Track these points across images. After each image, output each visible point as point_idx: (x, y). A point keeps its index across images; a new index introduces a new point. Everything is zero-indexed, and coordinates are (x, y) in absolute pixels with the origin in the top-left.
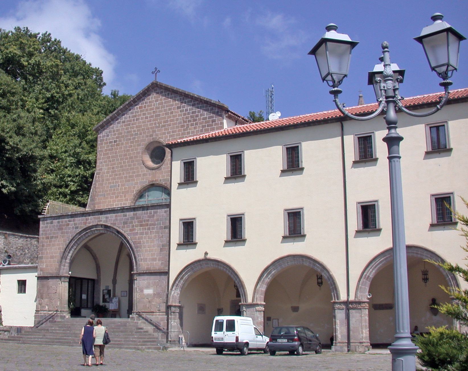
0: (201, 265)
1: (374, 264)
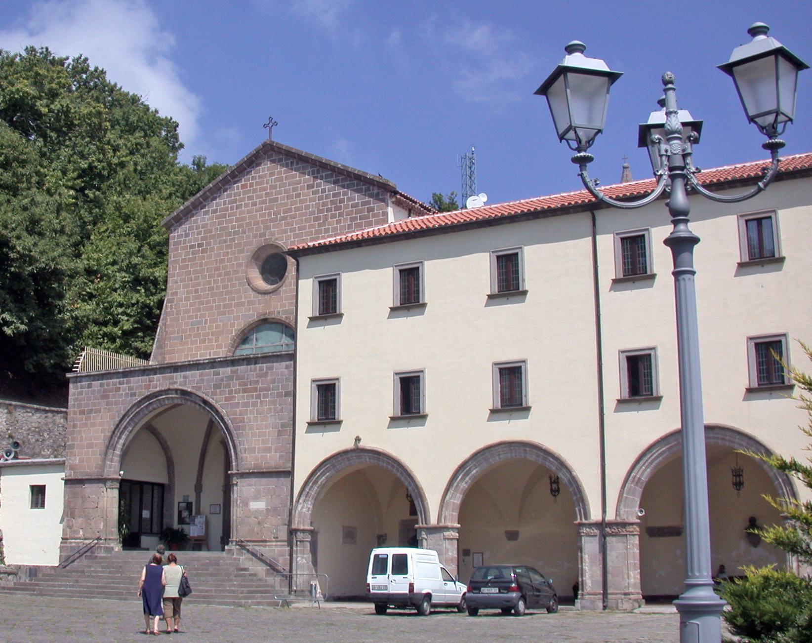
0: (348, 459)
1: (649, 458)
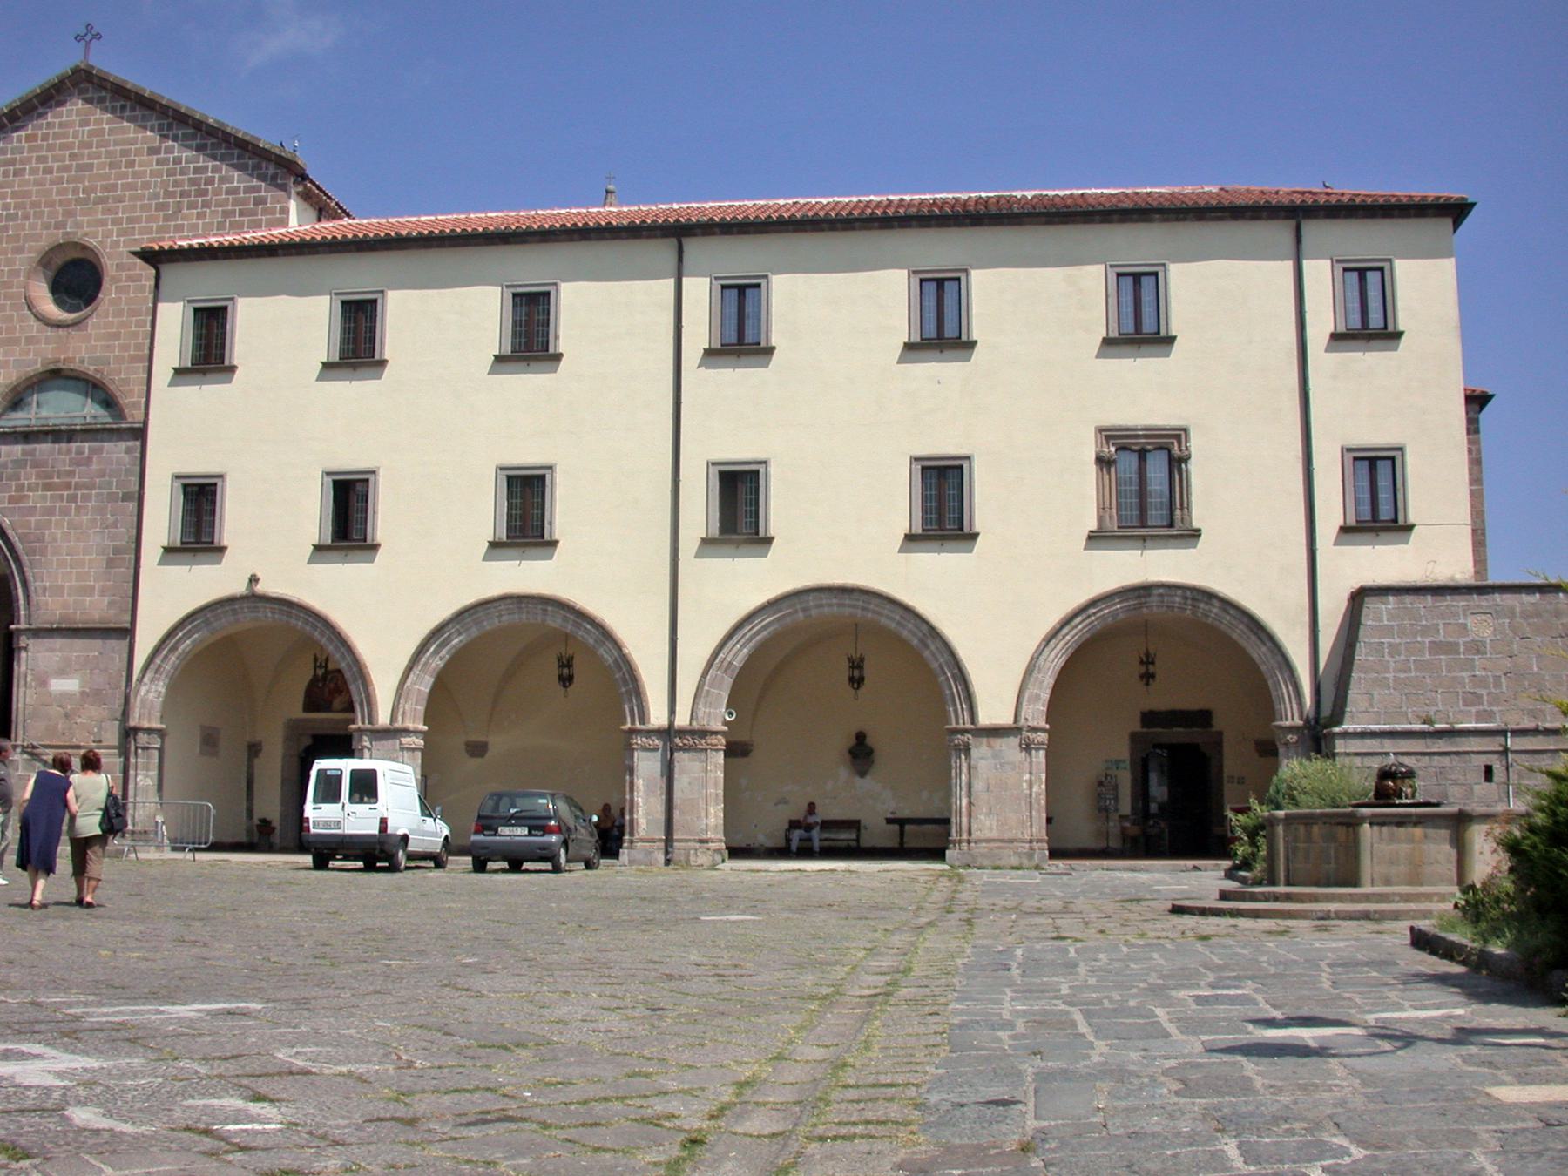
0: (235, 612)
1: (749, 631)
